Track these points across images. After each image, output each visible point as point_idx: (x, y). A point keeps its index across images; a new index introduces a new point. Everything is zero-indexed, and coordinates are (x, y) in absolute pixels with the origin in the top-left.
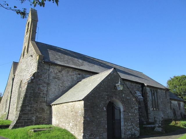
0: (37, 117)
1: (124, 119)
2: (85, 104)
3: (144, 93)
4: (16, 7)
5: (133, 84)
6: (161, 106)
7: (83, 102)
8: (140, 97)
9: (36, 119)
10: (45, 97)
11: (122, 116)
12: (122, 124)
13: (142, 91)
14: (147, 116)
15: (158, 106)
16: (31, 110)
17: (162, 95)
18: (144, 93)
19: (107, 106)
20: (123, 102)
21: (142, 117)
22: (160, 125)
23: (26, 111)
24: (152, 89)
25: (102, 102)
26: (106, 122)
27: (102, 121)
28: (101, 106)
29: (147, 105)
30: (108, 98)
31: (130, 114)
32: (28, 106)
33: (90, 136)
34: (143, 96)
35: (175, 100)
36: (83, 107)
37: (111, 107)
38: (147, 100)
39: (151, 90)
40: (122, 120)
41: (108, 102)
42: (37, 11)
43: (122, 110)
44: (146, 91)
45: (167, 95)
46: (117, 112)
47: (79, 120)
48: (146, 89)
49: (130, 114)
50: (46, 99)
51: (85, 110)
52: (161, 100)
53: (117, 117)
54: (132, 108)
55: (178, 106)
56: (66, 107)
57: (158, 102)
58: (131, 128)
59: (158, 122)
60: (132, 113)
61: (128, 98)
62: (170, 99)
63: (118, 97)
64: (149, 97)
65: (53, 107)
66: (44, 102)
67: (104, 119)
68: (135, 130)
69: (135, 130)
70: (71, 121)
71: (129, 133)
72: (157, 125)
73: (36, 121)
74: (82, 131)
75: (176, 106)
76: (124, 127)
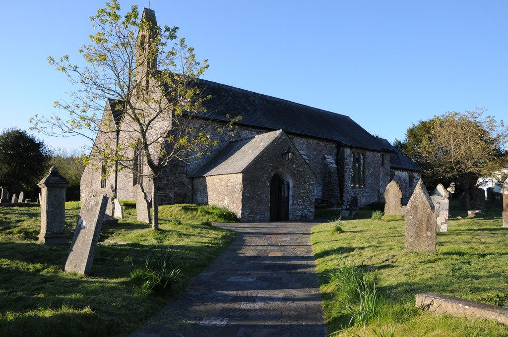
0: (175, 193)
1: (293, 196)
2: (243, 177)
3: (341, 158)
4: (118, 8)
5: (321, 143)
6: (370, 181)
7: (241, 176)
8: (331, 165)
9: (174, 196)
10: (184, 167)
11: (291, 193)
12: (291, 202)
13: (337, 154)
14: (342, 196)
15: (364, 180)
16: (167, 184)
17: (374, 161)
18: (341, 158)
19: (272, 179)
20: (293, 175)
21: (333, 197)
22: (348, 207)
23: (162, 186)
24: (356, 151)
25: (265, 175)
26: (269, 199)
27: (264, 198)
28: (263, 180)
29: (344, 178)
30: (272, 170)
31: (302, 191)
32: (164, 179)
33: (250, 213)
34: (337, 164)
35: (403, 170)
36: (241, 181)
37: (277, 183)
38: (343, 171)
39: (353, 153)
40: (291, 198)
41: (272, 174)
42: (156, 13)
43: (291, 185)
44: (344, 154)
45: (386, 161)
46: (284, 188)
47: (237, 195)
48: (344, 152)
49: (302, 191)
50: (186, 168)
51: (243, 184)
52: (372, 170)
53: (284, 194)
54: (305, 183)
55: (407, 180)
56: (218, 181)
57: (364, 173)
58: (303, 208)
59: (345, 203)
60: (304, 189)
61: (300, 169)
62: (391, 168)
63: (286, 169)
64: (348, 165)
65: (207, 179)
66: (184, 173)
67: (266, 196)
68: (308, 211)
69: (308, 211)
70: (226, 198)
71: (299, 214)
72: (344, 207)
73: (174, 199)
74: (240, 208)
75: (405, 181)
76: (293, 207)
